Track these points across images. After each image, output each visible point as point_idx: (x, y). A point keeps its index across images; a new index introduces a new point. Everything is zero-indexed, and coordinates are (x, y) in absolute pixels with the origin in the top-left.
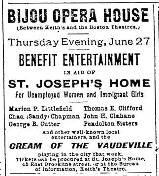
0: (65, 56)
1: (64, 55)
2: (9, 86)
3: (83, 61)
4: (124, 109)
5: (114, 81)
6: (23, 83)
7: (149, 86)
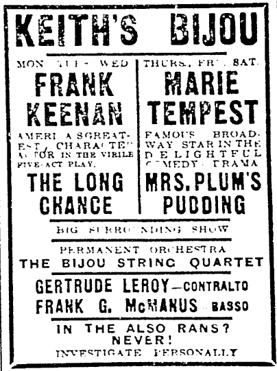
2: (212, 331)
5: (34, 261)
6: (133, 261)
7: (252, 265)
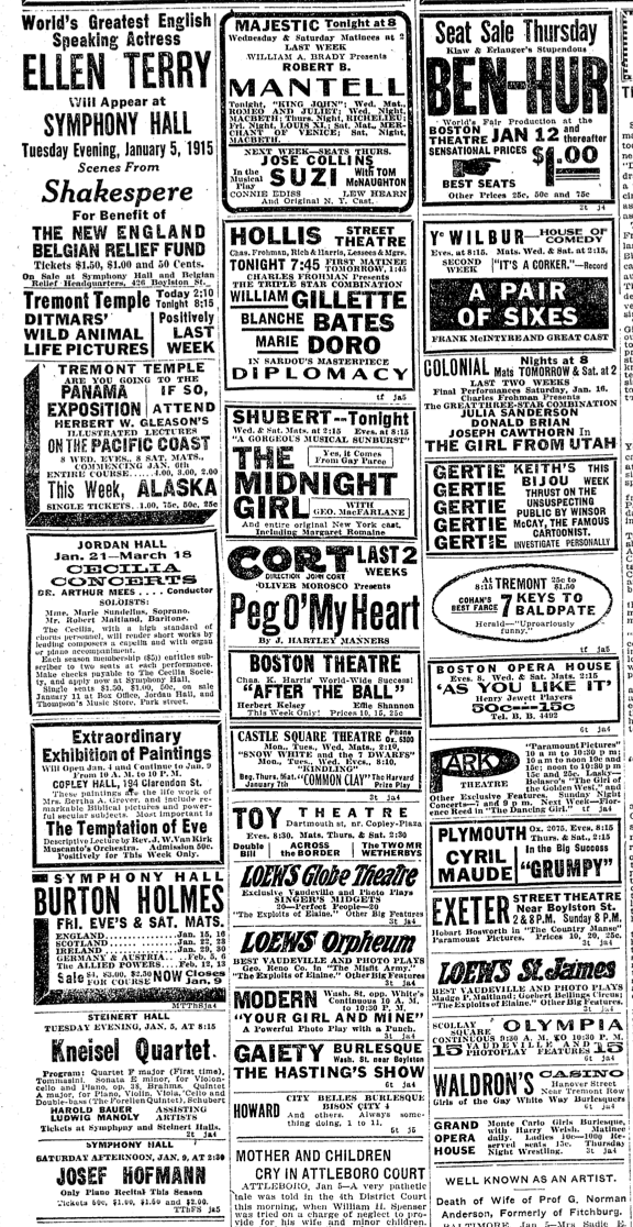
0: (31, 62)
1: (27, 58)
3: (31, 76)
4: (51, 79)
